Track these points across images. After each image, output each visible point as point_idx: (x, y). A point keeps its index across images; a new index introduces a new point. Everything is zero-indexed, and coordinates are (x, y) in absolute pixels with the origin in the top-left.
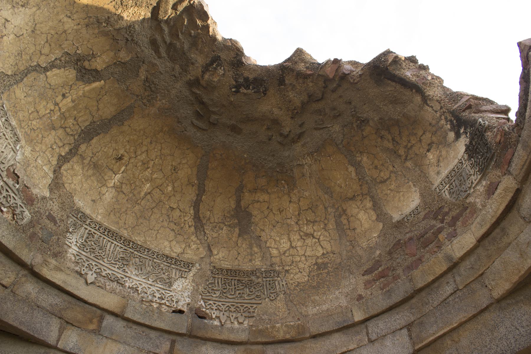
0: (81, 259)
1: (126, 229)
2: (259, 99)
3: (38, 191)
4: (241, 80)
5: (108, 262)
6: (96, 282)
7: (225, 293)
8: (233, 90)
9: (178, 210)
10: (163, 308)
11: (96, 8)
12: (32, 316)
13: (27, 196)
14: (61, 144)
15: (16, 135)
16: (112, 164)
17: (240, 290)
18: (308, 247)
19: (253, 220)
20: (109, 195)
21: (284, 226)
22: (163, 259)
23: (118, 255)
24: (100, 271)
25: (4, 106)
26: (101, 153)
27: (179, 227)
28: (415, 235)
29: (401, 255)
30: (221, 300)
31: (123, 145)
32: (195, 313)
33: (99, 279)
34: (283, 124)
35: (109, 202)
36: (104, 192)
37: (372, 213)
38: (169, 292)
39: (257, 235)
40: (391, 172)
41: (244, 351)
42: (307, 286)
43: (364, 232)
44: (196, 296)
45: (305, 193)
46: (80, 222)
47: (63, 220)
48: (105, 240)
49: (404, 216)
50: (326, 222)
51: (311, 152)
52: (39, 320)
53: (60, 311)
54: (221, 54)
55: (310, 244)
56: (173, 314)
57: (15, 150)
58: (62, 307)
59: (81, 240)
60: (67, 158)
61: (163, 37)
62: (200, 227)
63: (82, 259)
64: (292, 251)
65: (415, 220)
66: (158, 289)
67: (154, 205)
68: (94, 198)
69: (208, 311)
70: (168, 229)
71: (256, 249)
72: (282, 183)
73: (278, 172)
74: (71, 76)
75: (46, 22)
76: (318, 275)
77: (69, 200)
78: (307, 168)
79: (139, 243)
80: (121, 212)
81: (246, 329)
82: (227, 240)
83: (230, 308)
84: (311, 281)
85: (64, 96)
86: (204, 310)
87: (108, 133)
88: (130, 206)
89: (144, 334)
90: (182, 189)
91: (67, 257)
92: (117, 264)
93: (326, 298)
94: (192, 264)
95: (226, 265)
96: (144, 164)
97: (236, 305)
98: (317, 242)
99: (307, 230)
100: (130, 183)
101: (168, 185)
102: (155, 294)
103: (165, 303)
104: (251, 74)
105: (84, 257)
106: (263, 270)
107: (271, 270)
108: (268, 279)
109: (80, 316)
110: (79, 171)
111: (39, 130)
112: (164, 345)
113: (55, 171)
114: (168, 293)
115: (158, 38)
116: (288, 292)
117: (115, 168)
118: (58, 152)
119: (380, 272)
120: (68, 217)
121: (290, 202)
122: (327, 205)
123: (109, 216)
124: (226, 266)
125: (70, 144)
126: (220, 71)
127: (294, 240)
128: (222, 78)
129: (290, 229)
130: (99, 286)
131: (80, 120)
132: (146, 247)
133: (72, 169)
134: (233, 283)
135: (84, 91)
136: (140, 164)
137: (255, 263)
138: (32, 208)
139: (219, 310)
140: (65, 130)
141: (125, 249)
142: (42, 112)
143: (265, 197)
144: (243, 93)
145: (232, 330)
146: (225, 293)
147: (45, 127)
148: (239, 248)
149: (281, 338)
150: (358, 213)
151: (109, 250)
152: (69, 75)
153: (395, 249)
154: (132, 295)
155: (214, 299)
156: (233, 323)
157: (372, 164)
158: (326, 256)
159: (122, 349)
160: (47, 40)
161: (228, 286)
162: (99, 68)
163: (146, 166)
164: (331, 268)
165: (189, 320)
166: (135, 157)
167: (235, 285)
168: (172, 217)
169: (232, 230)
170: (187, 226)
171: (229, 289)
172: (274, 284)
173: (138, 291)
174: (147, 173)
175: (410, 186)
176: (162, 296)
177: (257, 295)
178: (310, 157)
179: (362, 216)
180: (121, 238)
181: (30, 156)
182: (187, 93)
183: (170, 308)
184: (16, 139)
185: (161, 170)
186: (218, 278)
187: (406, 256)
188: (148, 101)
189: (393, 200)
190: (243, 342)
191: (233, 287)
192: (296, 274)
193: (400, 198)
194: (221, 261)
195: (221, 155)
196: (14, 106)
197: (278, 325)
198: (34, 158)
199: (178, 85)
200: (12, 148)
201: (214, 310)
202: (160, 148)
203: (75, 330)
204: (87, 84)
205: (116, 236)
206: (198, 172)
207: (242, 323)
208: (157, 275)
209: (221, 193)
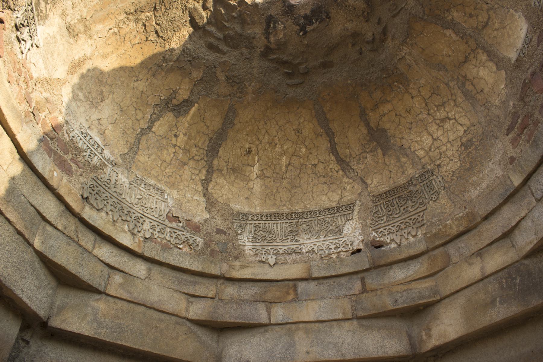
1: (284, 205)
2: (327, 25)
4: (302, 21)
5: (281, 241)
6: (278, 261)
7: (391, 215)
8: (301, 34)
9: (321, 164)
11: (150, 58)
14: (197, 172)
15: (159, 189)
18: (449, 132)
19: (389, 134)
20: (257, 186)
21: (419, 123)
24: (277, 251)
25: (137, 176)
27: (328, 178)
28: (536, 68)
29: (532, 96)
32: (372, 246)
33: (279, 258)
34: (363, 32)
35: (260, 192)
36: (252, 187)
37: (490, 64)
38: (341, 239)
39: (399, 145)
40: (488, 10)
41: (428, 260)
42: (462, 171)
43: (492, 88)
44: (367, 230)
45: (421, 82)
46: (243, 222)
47: (230, 228)
48: (270, 225)
49: (519, 52)
50: (454, 98)
51: (403, 41)
54: (270, 12)
55: (449, 129)
56: (353, 255)
58: (261, 293)
59: (251, 236)
60: (208, 179)
61: (214, 36)
62: (347, 167)
64: (437, 144)
65: (530, 50)
67: (298, 171)
68: (246, 196)
69: (382, 239)
70: (320, 185)
71: (403, 160)
72: (396, 85)
73: (385, 78)
74: (170, 119)
75: (124, 97)
76: (468, 155)
77: (227, 210)
78: (409, 57)
79: (300, 210)
80: (274, 194)
81: (422, 239)
82: (375, 165)
83: (400, 226)
84: (463, 165)
85: (176, 136)
86: (378, 239)
88: (278, 185)
89: (336, 283)
90: (314, 144)
91: (246, 255)
93: (483, 175)
94: (352, 204)
95: (383, 188)
96: (271, 143)
98: (455, 123)
99: (440, 115)
101: (300, 148)
102: (330, 247)
104: (306, 9)
106: (417, 176)
107: (424, 173)
108: (425, 182)
109: (278, 294)
112: (356, 286)
113: (204, 195)
115: (212, 40)
116: (447, 186)
118: (198, 179)
119: (521, 124)
120: (232, 223)
121: (412, 98)
122: (447, 81)
123: (265, 203)
124: (383, 190)
125: (204, 167)
126: (280, 26)
127: (433, 132)
128: (286, 31)
129: (425, 124)
131: (200, 144)
132: (307, 211)
134: (395, 202)
135: (188, 121)
136: (268, 145)
138: (201, 233)
139: (392, 233)
140: (194, 159)
141: (290, 223)
142: (168, 159)
143: (389, 107)
144: (311, 30)
145: (409, 246)
146: (391, 215)
148: (389, 166)
149: (456, 233)
150: (478, 71)
151: (277, 231)
152: (168, 119)
153: (524, 93)
155: (383, 225)
157: (465, 14)
158: (468, 132)
160: (135, 108)
161: (391, 207)
162: (186, 97)
163: (273, 144)
164: (477, 142)
165: (368, 255)
169: (375, 153)
170: (335, 172)
171: (393, 209)
172: (431, 185)
173: (315, 251)
175: (512, 14)
177: (420, 203)
178: (405, 46)
179: (483, 73)
181: (179, 197)
182: (268, 64)
185: (287, 139)
186: (380, 204)
187: (537, 95)
188: (241, 93)
189: (503, 39)
190: (423, 252)
191: (396, 206)
192: (448, 163)
193: (508, 33)
194: (377, 187)
195: (329, 95)
196: (145, 170)
197: (449, 222)
198: (183, 196)
199: (255, 63)
201: (387, 235)
202: (275, 123)
204: (186, 115)
205: (278, 216)
206: (318, 121)
207: (416, 235)
208: (326, 230)
209: (349, 127)
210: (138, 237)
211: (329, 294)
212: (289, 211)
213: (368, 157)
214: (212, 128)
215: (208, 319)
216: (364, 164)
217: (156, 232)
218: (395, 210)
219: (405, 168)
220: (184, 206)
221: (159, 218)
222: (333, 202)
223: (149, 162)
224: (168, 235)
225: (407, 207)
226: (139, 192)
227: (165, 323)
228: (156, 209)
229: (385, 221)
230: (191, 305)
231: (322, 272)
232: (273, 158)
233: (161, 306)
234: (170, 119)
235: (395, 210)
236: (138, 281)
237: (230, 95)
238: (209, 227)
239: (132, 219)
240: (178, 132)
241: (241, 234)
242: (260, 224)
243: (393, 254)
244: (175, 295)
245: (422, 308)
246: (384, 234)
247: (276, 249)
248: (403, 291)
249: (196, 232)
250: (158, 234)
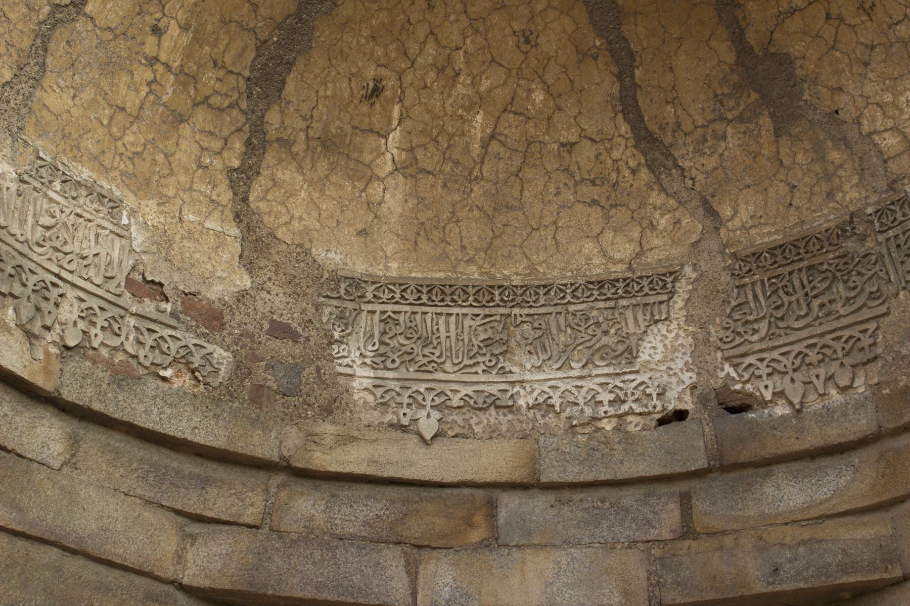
0: (388, 390)
1: (471, 261)
3: (220, 287)
5: (456, 368)
6: (445, 427)
7: (782, 319)
9: (586, 143)
10: (631, 423)
12: (335, 564)
13: (201, 315)
14: (217, 145)
15: (104, 197)
16: (364, 115)
17: (822, 293)
19: (799, 72)
21: (894, 50)
22: (592, 295)
23: (474, 340)
24: (444, 398)
25: (41, 155)
26: (324, 105)
27: (606, 186)
30: (777, 344)
31: (365, 54)
32: (720, 404)
33: (450, 419)
35: (402, 215)
36: (378, 198)
38: (632, 377)
41: (877, 461)
44: (708, 357)
46: (350, 306)
47: (310, 321)
52: (355, 565)
53: (391, 529)
56: (661, 428)
57: (119, 231)
59: (370, 348)
60: (250, 167)
62: (663, 158)
63: (392, 390)
66: (603, 380)
67: (517, 161)
68: (360, 226)
69: (749, 386)
70: (579, 207)
71: (835, 156)
77: (302, 265)
79: (517, 281)
80: (442, 224)
81: (866, 398)
83: (806, 355)
85: (156, 31)
86: (738, 387)
87: (311, 48)
88: (457, 197)
89: (607, 504)
90: (572, 81)
92: (478, 363)
94: (671, 273)
97: (820, 341)
100: (432, 139)
101: (530, 91)
102: (599, 398)
103: (631, 408)
105: (394, 383)
106: (870, 210)
107: (893, 204)
108: (891, 233)
109: (440, 523)
110: (294, 179)
111: (148, 147)
113: (237, 216)
114: (633, 381)
117: (377, 121)
118: (220, 166)
120: (317, 307)
124: (766, 240)
125: (239, 130)
130: (456, 436)
131: (228, 59)
132: (537, 283)
133: (274, 185)
134: (797, 283)
136: (432, 74)
137: (844, 196)
138: (225, 333)
139: (779, 372)
140: (210, 106)
142: (132, 101)
145: (828, 415)
146: (782, 319)
147: (158, 132)
151: (448, 337)
154: (542, 422)
155: (757, 347)
156: (824, 394)
159: (564, 560)
163: (449, 72)
165: (707, 430)
166: (412, 66)
167: (804, 287)
169: (752, 126)
170: (627, 173)
171: (790, 303)
173: (553, 406)
174: (462, 89)
176: (618, 395)
177: (871, 293)
180: (466, 293)
181: (162, 220)
183: (649, 418)
184: (111, 204)
185: (493, 60)
191: (800, 294)
194: (748, 230)
196: (64, 136)
200: (111, 231)
203: (441, 556)
205: (453, 293)
206: (591, 13)
207: (850, 387)
208: (588, 344)
209: (680, 39)
210: (44, 343)
211: (588, 533)
212: (485, 281)
213: (729, 136)
214: (269, 11)
215: (239, 587)
217: (98, 331)
218: (794, 306)
219: (837, 181)
220: (176, 248)
221: (106, 286)
222: (615, 263)
223: (76, 112)
224: (131, 338)
225: (831, 302)
226: (45, 206)
227: (115, 596)
228: (96, 260)
229: (763, 335)
230: (192, 545)
231: (570, 468)
233: (108, 547)
235: (794, 306)
236: (40, 475)
238: (248, 314)
239: (28, 292)
240: (165, 19)
241: (341, 342)
242: (399, 312)
243: (778, 434)
244: (146, 514)
245: (847, 595)
246: (757, 373)
247: (442, 393)
248: (799, 544)
249: (212, 329)
250: (101, 337)
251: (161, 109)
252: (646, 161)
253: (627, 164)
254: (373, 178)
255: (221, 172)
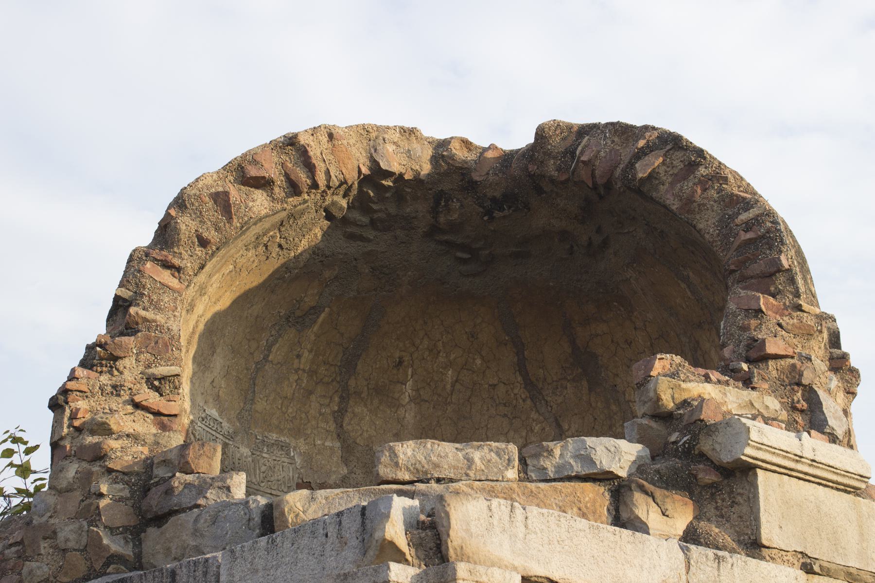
3: (334, 477)
4: (488, 204)
8: (486, 218)
14: (327, 401)
36: (403, 416)
68: (395, 431)
71: (614, 407)
77: (369, 456)
80: (433, 428)
88: (440, 413)
96: (432, 350)
101: (474, 359)
125: (337, 391)
131: (330, 360)
136: (427, 353)
162: (313, 304)
168: (498, 397)
170: (521, 401)
174: (442, 359)
184: (286, 449)
185: (456, 345)
198: (311, 445)
213: (568, 387)
216: (562, 396)
223: (268, 408)
232: (434, 371)
234: (291, 336)
237: (375, 290)
251: (302, 391)
252: (530, 395)
253: (521, 396)
254: (400, 406)
255: (330, 414)
